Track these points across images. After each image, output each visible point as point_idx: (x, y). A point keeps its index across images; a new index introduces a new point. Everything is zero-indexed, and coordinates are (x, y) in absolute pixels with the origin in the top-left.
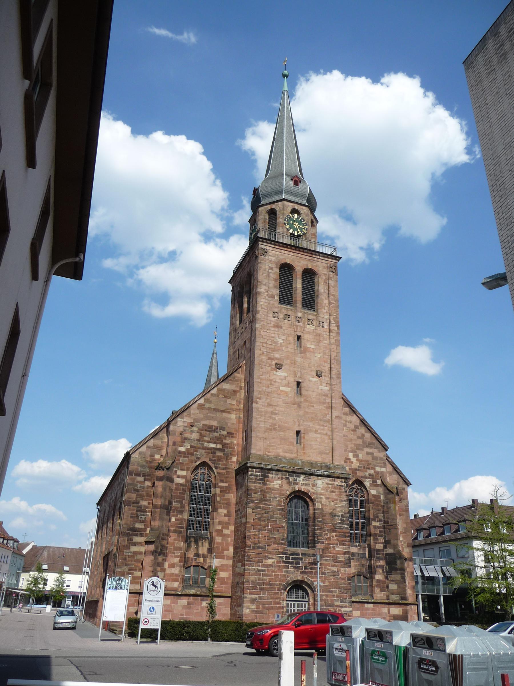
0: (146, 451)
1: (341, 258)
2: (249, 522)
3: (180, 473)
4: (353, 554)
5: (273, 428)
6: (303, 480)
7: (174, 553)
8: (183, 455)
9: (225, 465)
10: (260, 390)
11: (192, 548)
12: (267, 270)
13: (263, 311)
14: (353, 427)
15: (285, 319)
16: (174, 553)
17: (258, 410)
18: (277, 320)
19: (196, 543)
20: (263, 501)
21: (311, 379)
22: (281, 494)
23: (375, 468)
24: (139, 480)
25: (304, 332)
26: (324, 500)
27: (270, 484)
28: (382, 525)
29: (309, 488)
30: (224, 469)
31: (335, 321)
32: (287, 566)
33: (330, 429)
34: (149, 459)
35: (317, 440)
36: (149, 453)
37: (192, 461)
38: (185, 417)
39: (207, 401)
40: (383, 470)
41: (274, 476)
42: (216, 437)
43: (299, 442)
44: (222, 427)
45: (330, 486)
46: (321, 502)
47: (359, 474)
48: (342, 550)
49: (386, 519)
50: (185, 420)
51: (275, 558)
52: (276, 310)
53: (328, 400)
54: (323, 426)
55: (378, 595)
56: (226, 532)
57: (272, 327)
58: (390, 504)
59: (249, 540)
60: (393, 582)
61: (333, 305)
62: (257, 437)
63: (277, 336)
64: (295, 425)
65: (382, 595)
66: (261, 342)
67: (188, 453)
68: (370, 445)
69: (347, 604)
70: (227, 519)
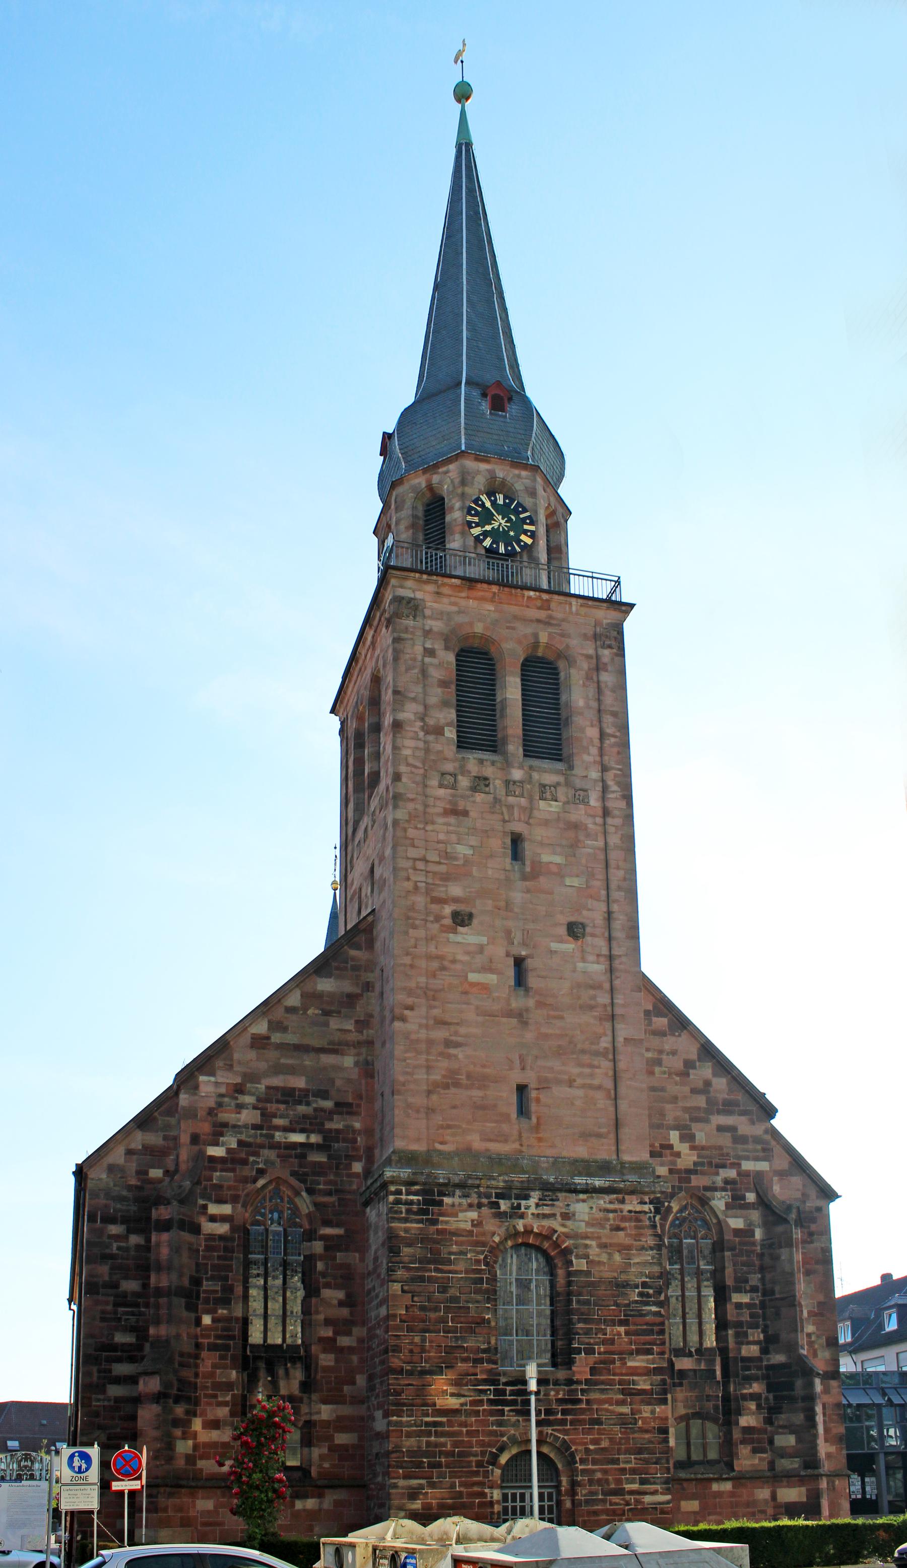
0: (125, 1162)
1: (632, 606)
2: (395, 1316)
3: (214, 1209)
4: (682, 1373)
5: (451, 1081)
6: (537, 1205)
7: (215, 1396)
8: (219, 1166)
9: (334, 1183)
10: (412, 984)
11: (260, 1384)
12: (419, 658)
13: (412, 773)
14: (679, 1065)
15: (474, 789)
16: (215, 1396)
17: (407, 1038)
18: (453, 796)
19: (271, 1371)
20: (429, 1262)
21: (554, 946)
22: (477, 1244)
23: (739, 1165)
24: (114, 1232)
25: (531, 821)
26: (594, 1251)
27: (447, 1222)
28: (757, 1298)
29: (555, 1224)
30: (329, 1193)
31: (618, 784)
32: (499, 1410)
33: (611, 1073)
34: (133, 1182)
35: (573, 1104)
36: (133, 1167)
37: (245, 1180)
38: (219, 1073)
39: (277, 1026)
40: (763, 1166)
41: (457, 1200)
42: (305, 1117)
43: (523, 1110)
44: (319, 1091)
45: (611, 1215)
46: (586, 1256)
47: (697, 1181)
48: (644, 1364)
49: (769, 1286)
50: (220, 1080)
51: (466, 1394)
52: (449, 767)
53: (604, 999)
54: (591, 1066)
55: (747, 1462)
56: (344, 1341)
57: (438, 815)
58: (780, 1247)
59: (399, 1358)
60: (785, 1431)
61: (613, 740)
62: (409, 1106)
63: (454, 837)
64: (511, 1069)
65: (757, 1461)
66: (408, 858)
67: (231, 1161)
68: (728, 1107)
69: (658, 1487)
70: (345, 1312)
